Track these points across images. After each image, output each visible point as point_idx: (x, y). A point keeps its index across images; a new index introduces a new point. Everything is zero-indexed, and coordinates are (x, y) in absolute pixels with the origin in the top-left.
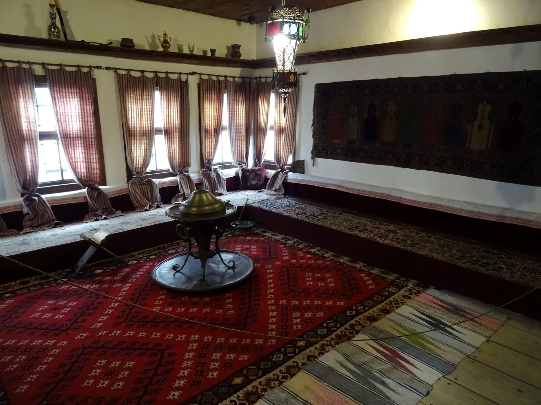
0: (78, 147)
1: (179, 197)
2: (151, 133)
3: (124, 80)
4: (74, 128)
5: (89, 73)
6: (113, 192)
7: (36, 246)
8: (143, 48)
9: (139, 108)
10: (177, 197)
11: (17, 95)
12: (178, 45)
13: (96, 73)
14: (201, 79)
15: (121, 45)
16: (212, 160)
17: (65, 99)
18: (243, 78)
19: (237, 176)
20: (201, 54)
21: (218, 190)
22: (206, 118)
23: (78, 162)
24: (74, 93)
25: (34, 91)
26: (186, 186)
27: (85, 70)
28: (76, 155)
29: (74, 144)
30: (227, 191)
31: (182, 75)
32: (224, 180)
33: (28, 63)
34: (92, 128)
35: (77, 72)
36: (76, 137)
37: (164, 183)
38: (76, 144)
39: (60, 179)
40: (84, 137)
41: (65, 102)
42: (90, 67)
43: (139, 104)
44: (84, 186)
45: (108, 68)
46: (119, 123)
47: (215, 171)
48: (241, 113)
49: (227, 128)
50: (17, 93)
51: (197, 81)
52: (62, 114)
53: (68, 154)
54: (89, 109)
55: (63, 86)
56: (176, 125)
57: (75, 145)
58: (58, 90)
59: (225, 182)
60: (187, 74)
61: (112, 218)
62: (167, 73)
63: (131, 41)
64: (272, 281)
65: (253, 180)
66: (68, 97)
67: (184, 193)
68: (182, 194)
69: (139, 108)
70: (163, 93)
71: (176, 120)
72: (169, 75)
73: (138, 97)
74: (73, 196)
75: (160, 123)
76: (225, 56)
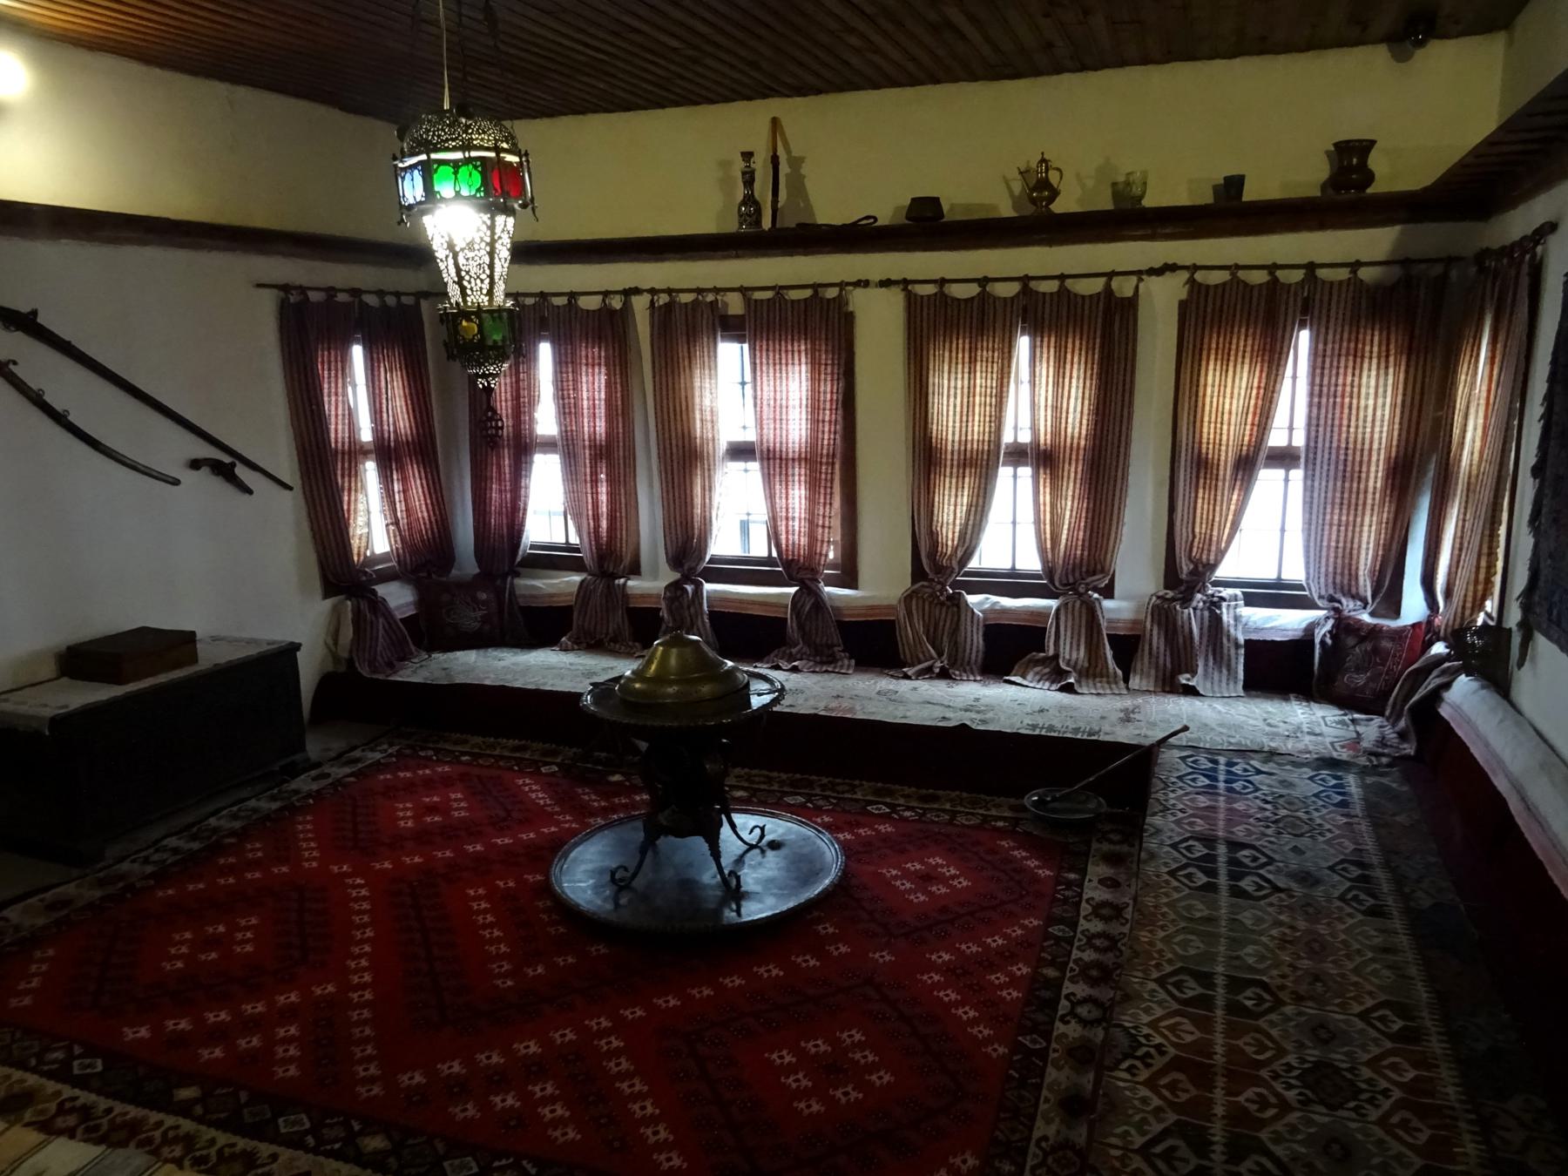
0: (797, 484)
1: (1038, 662)
2: (988, 460)
3: (925, 310)
4: (790, 437)
5: (841, 302)
6: (856, 608)
7: (570, 684)
8: (996, 215)
9: (959, 385)
10: (1030, 661)
11: (690, 362)
12: (1114, 184)
13: (859, 300)
14: (1192, 281)
15: (907, 218)
16: (1213, 567)
17: (778, 367)
18: (1405, 262)
19: (1302, 644)
20: (1105, 203)
21: (1194, 673)
22: (1206, 419)
23: (793, 518)
24: (799, 352)
25: (715, 352)
26: (1076, 636)
27: (832, 293)
28: (790, 501)
29: (787, 475)
30: (1246, 687)
31: (1114, 278)
32: (1237, 646)
33: (716, 290)
34: (829, 437)
35: (1228, 288)
36: (793, 460)
37: (1005, 611)
38: (793, 475)
39: (1008, 566)
40: (811, 459)
41: (778, 375)
42: (842, 285)
43: (960, 376)
44: (791, 578)
45: (886, 283)
46: (907, 428)
47: (1214, 604)
48: (1371, 402)
49: (1298, 458)
50: (690, 357)
51: (1183, 294)
52: (765, 403)
53: (771, 497)
54: (828, 388)
55: (765, 335)
56: (1072, 438)
57: (790, 478)
58: (764, 347)
59: (1242, 651)
60: (1139, 273)
61: (826, 671)
62: (1062, 277)
63: (935, 201)
64: (366, 918)
65: (1358, 670)
66: (784, 361)
67: (1056, 657)
68: (1047, 658)
69: (959, 385)
70: (1039, 339)
71: (1077, 419)
72: (1069, 283)
73: (960, 355)
74: (761, 599)
75: (1018, 428)
76: (1319, 194)
